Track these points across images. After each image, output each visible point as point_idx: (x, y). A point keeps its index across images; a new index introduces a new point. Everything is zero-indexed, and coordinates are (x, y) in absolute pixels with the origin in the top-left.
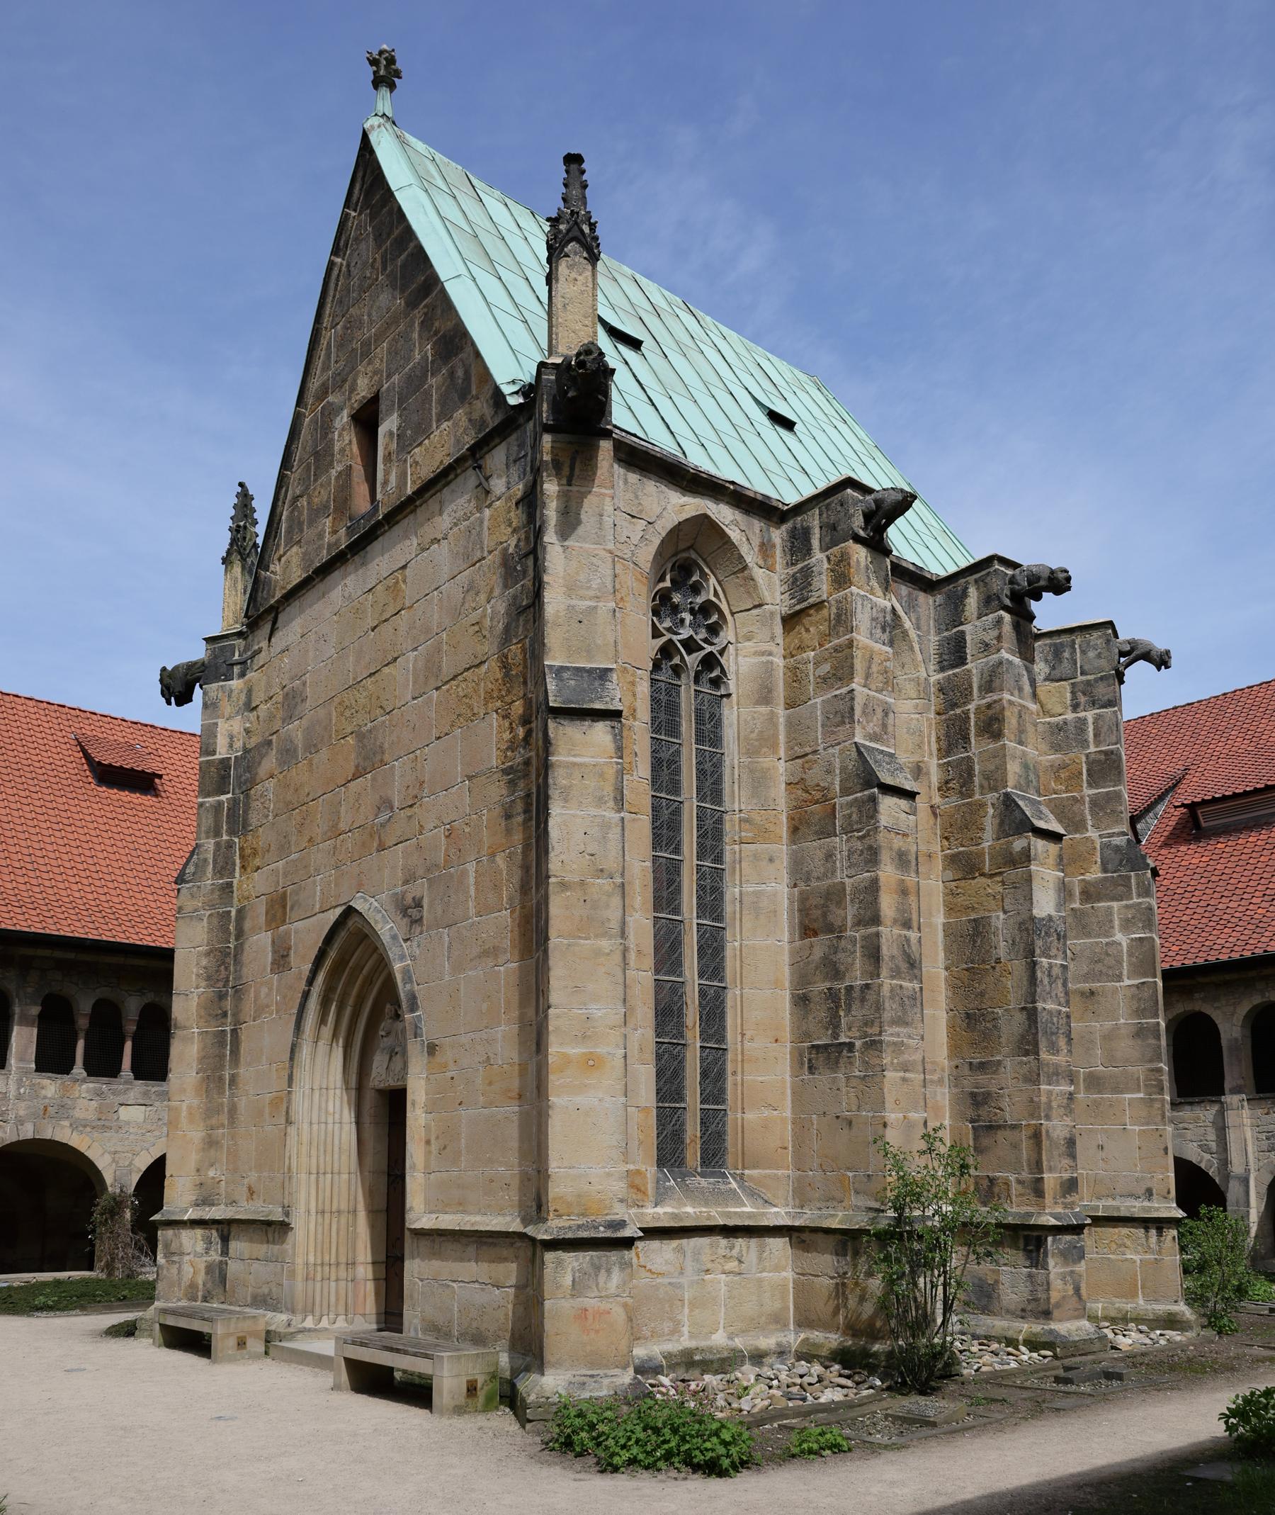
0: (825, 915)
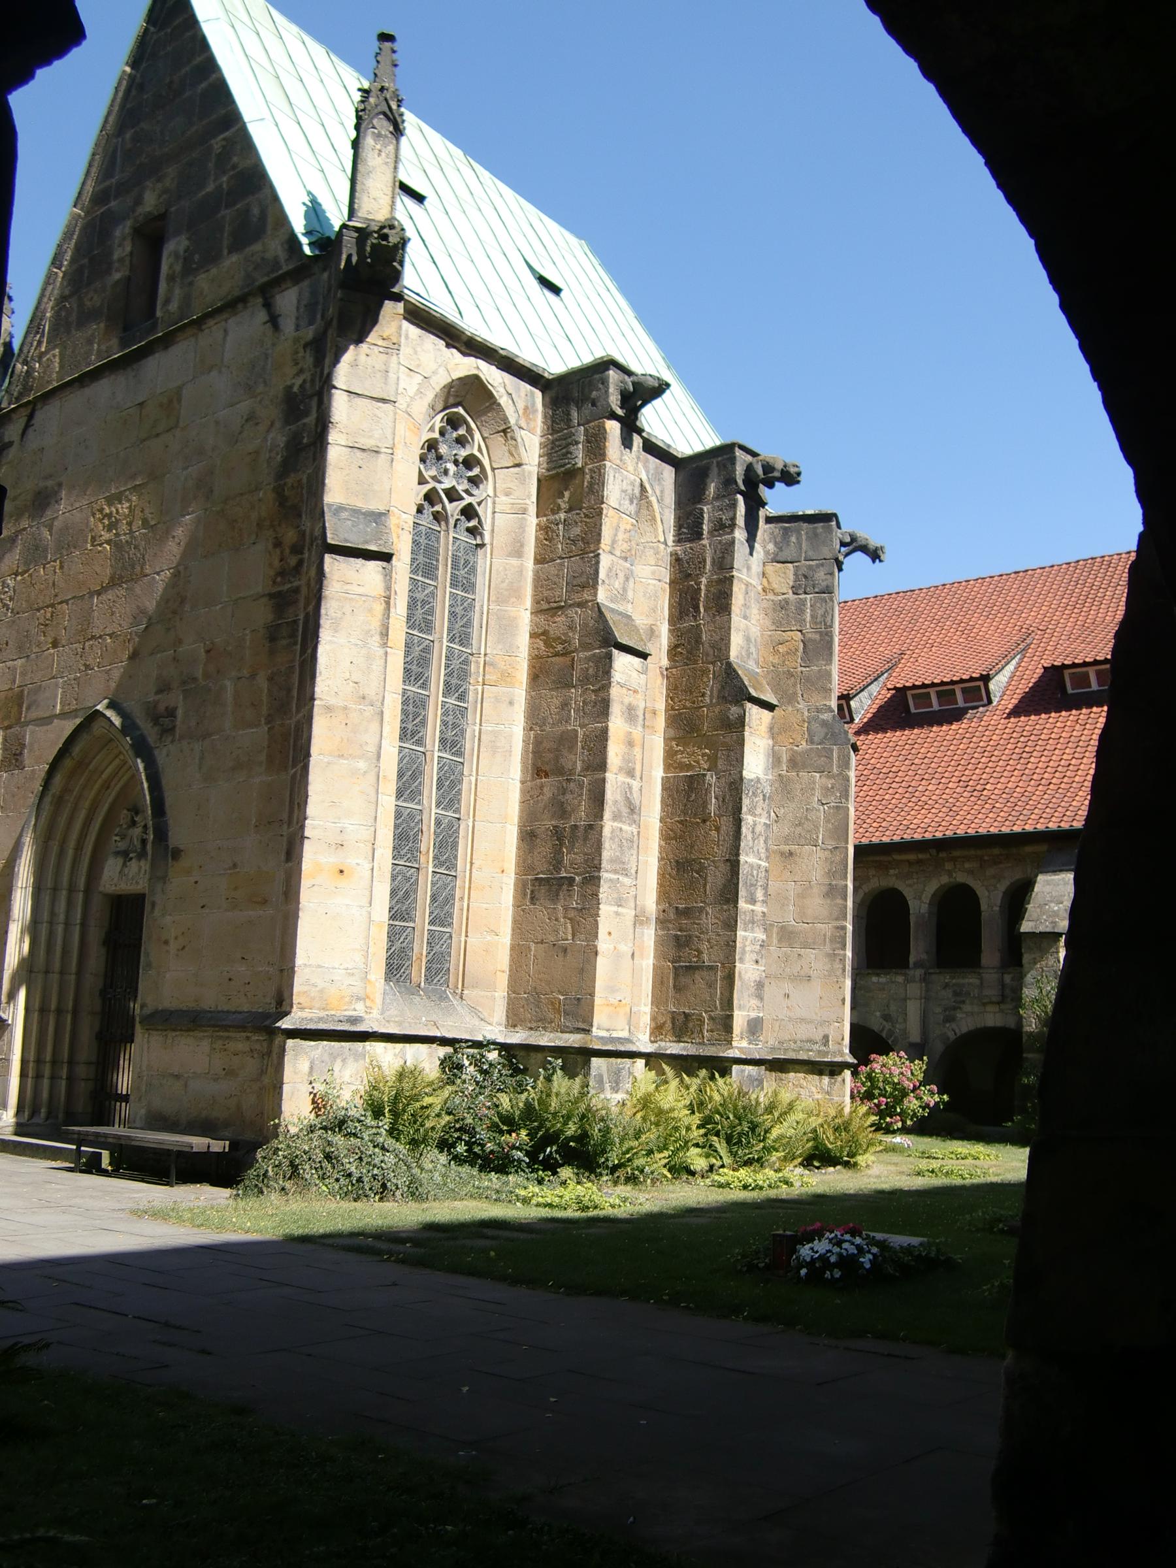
0: (557, 759)
